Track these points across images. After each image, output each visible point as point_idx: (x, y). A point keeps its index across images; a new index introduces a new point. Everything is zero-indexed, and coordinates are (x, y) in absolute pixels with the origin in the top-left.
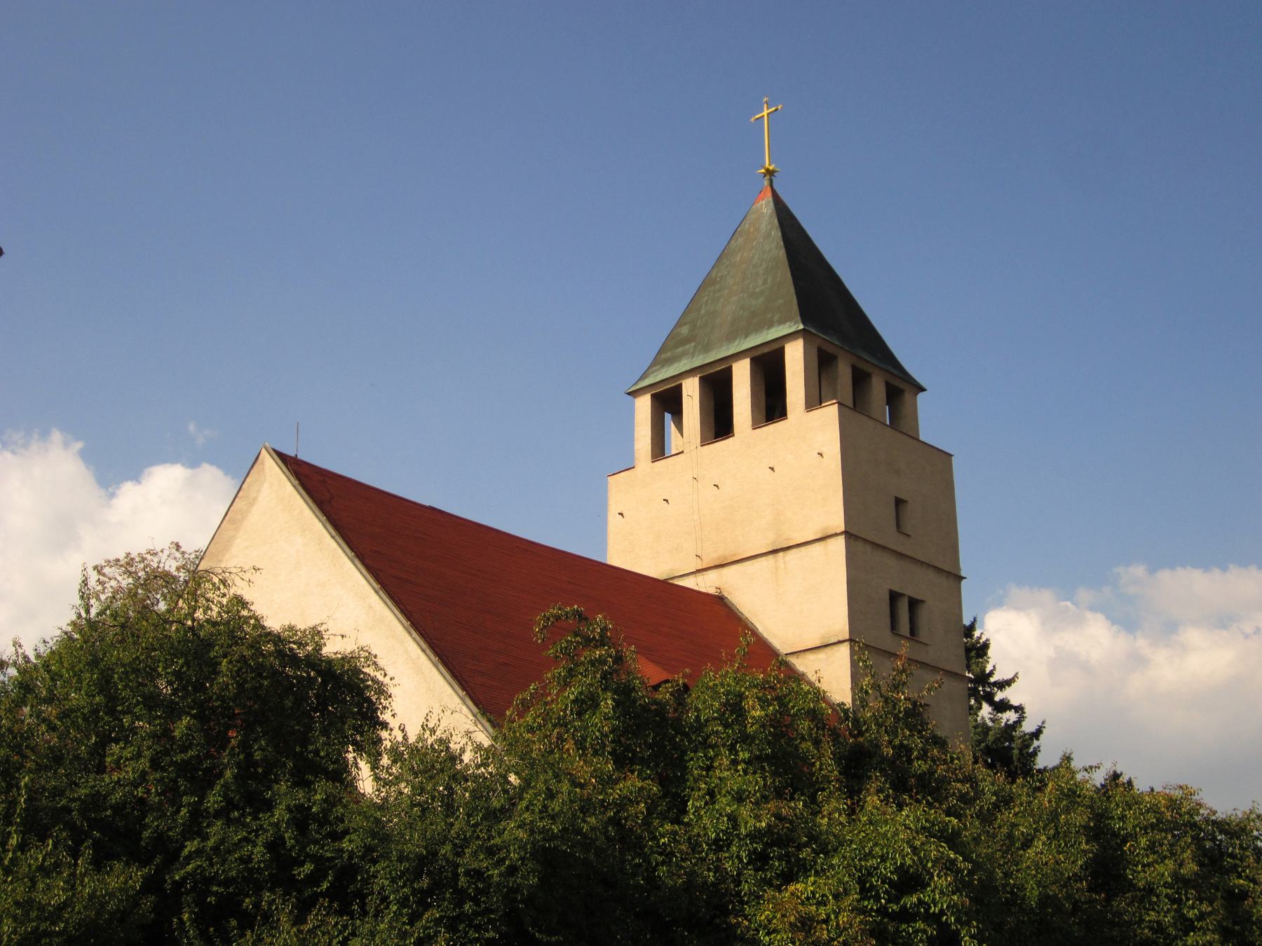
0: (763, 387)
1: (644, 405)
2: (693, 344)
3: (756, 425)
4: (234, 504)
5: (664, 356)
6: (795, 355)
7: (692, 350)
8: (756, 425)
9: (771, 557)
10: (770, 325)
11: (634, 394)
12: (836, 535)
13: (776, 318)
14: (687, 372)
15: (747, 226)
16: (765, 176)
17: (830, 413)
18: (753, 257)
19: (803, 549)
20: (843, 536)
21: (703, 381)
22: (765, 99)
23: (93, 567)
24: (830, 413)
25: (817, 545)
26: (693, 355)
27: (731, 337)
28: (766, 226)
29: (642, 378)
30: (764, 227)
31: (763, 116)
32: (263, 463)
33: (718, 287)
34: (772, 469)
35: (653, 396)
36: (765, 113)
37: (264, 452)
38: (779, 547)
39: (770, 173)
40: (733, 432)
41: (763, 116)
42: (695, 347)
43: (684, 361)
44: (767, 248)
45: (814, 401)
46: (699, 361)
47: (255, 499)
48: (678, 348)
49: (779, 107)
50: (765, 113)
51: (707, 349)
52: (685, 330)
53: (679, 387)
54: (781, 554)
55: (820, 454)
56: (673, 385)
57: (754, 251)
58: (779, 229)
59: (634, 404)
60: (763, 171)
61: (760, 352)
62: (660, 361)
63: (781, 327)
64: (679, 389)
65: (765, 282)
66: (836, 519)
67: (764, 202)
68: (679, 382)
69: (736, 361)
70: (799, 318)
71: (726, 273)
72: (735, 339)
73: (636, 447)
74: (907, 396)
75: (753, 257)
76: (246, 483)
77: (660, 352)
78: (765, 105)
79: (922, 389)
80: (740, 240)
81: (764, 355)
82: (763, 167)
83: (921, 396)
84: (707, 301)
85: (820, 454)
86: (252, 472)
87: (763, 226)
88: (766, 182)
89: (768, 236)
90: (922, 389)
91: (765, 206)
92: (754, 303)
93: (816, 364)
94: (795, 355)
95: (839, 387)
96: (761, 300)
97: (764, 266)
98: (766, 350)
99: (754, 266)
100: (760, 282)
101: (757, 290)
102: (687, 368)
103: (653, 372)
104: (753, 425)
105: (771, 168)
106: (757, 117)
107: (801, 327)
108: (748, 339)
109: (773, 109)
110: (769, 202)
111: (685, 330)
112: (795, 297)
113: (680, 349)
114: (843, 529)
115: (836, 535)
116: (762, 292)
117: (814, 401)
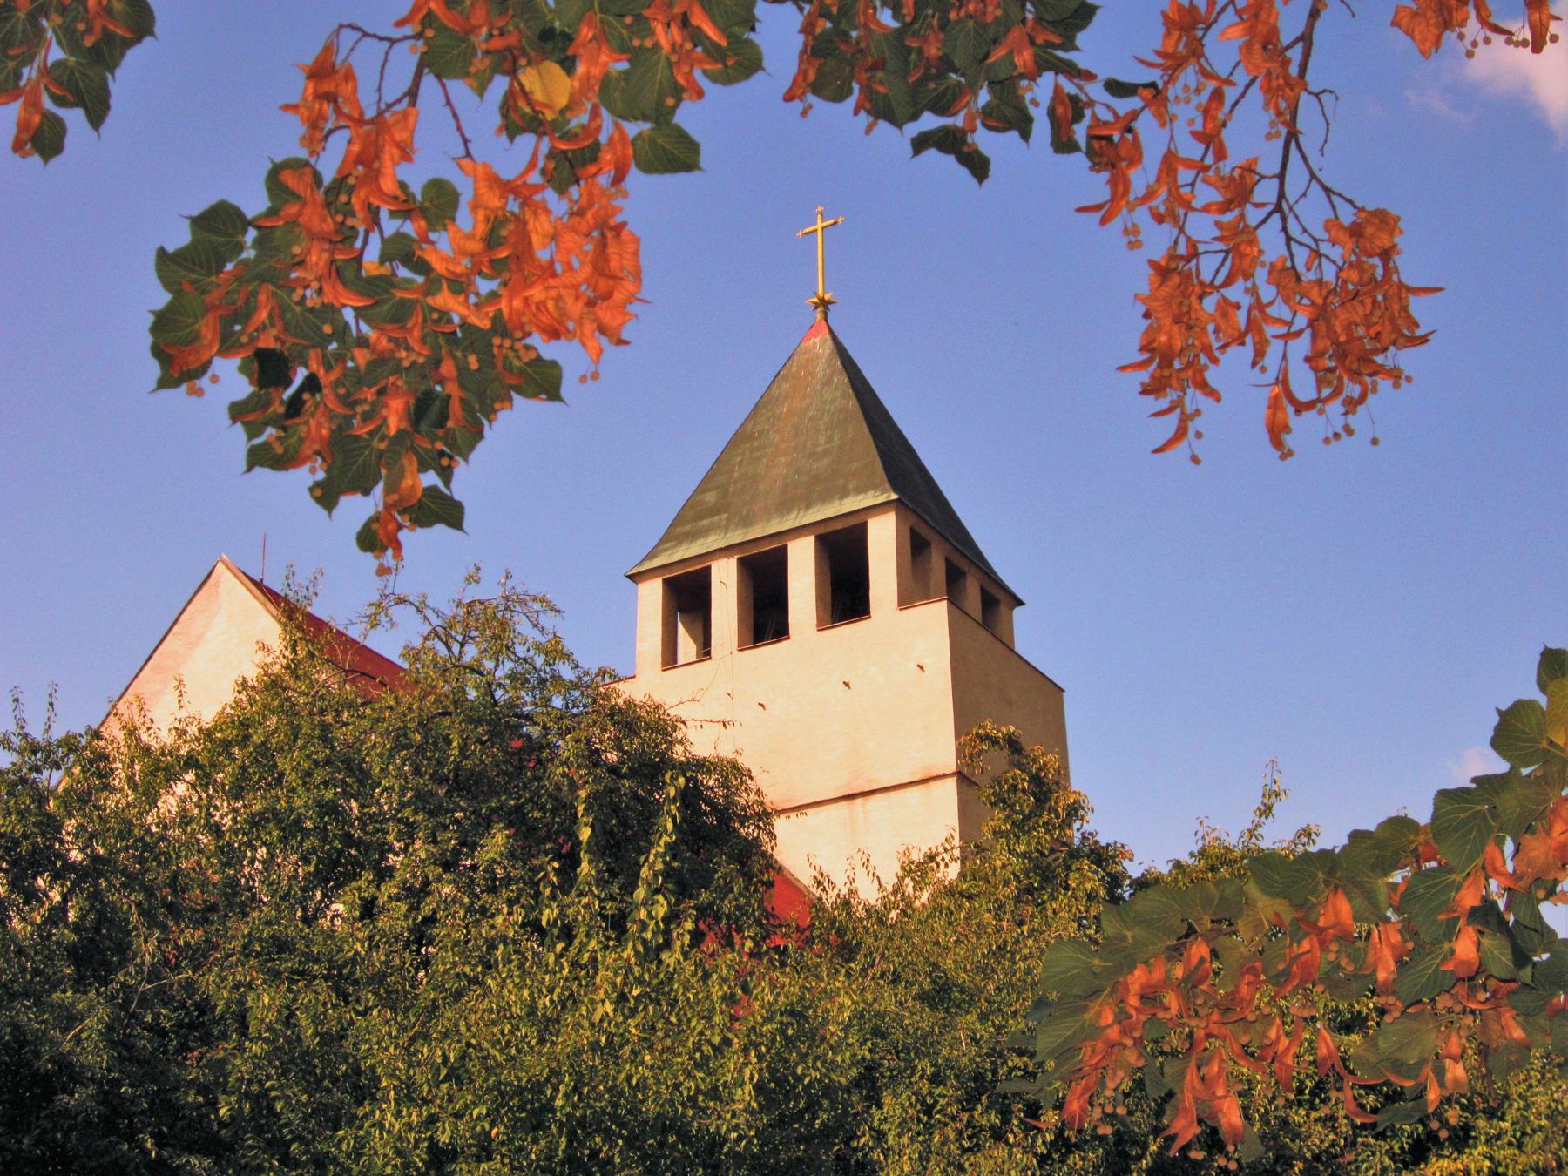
0: (829, 577)
1: (652, 594)
2: (725, 516)
3: (822, 625)
4: (165, 643)
5: (678, 530)
6: (883, 538)
7: (723, 523)
8: (822, 625)
9: (843, 805)
10: (844, 494)
11: (635, 578)
12: (944, 776)
13: (851, 486)
14: (721, 550)
15: (794, 370)
16: (816, 308)
17: (936, 614)
18: (807, 408)
19: (893, 794)
20: (955, 778)
21: (743, 564)
22: (819, 209)
23: (1139, 247)
24: (936, 614)
25: (915, 789)
26: (727, 529)
27: (784, 507)
28: (824, 370)
29: (651, 556)
30: (820, 369)
31: (816, 231)
32: (217, 585)
33: (756, 444)
34: (847, 685)
35: (666, 581)
36: (819, 226)
37: (220, 567)
38: (856, 791)
39: (824, 304)
40: (787, 633)
41: (816, 231)
42: (728, 520)
43: (712, 538)
44: (828, 396)
45: (906, 599)
46: (736, 537)
47: (200, 637)
48: (702, 519)
49: (840, 220)
50: (819, 226)
51: (747, 522)
52: (711, 497)
53: (708, 570)
54: (859, 801)
55: (920, 667)
56: (691, 569)
57: (808, 401)
58: (844, 374)
59: (636, 591)
60: (816, 300)
61: (823, 530)
62: (673, 536)
63: (861, 497)
64: (705, 574)
65: (830, 439)
66: (947, 759)
67: (817, 340)
68: (706, 564)
69: (795, 538)
70: (887, 486)
71: (767, 427)
72: (789, 511)
73: (638, 649)
74: (1003, 608)
75: (807, 408)
76: (185, 613)
77: (673, 525)
78: (819, 216)
79: (1021, 603)
80: (786, 386)
81: (836, 532)
82: (816, 294)
83: (1017, 611)
84: (741, 461)
85: (920, 667)
86: (198, 596)
87: (820, 368)
88: (819, 315)
89: (828, 382)
90: (1021, 603)
91: (821, 346)
92: (815, 465)
93: (908, 548)
94: (883, 538)
95: (932, 584)
96: (825, 462)
97: (826, 419)
98: (839, 526)
99: (812, 419)
100: (822, 439)
101: (819, 449)
102: (722, 545)
103: (666, 550)
104: (818, 625)
105: (827, 297)
106: (807, 230)
107: (894, 496)
108: (811, 511)
109: (832, 221)
110: (825, 341)
111: (711, 497)
112: (878, 459)
113: (705, 522)
114: (953, 768)
115: (944, 776)
116: (826, 453)
117: (906, 599)
